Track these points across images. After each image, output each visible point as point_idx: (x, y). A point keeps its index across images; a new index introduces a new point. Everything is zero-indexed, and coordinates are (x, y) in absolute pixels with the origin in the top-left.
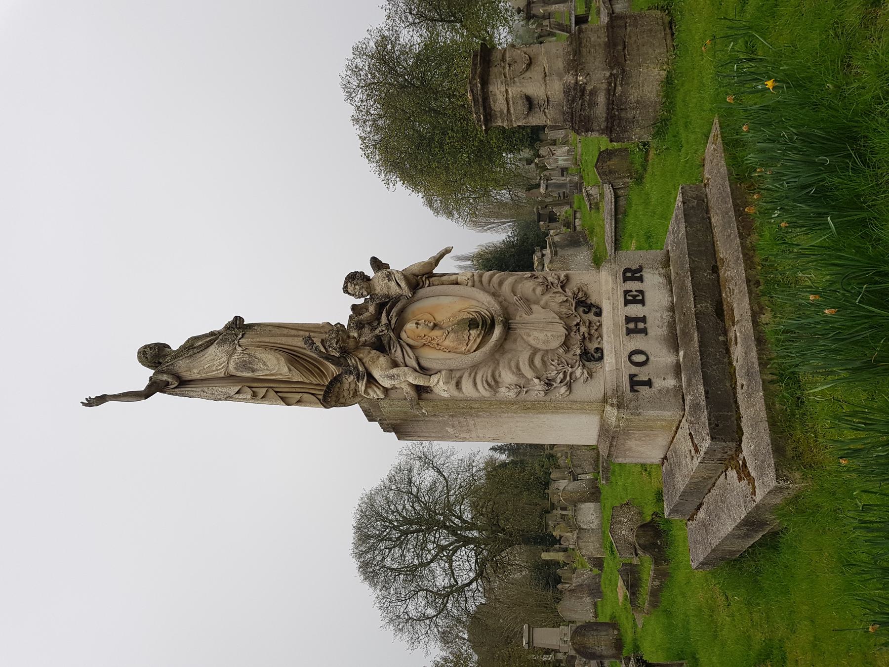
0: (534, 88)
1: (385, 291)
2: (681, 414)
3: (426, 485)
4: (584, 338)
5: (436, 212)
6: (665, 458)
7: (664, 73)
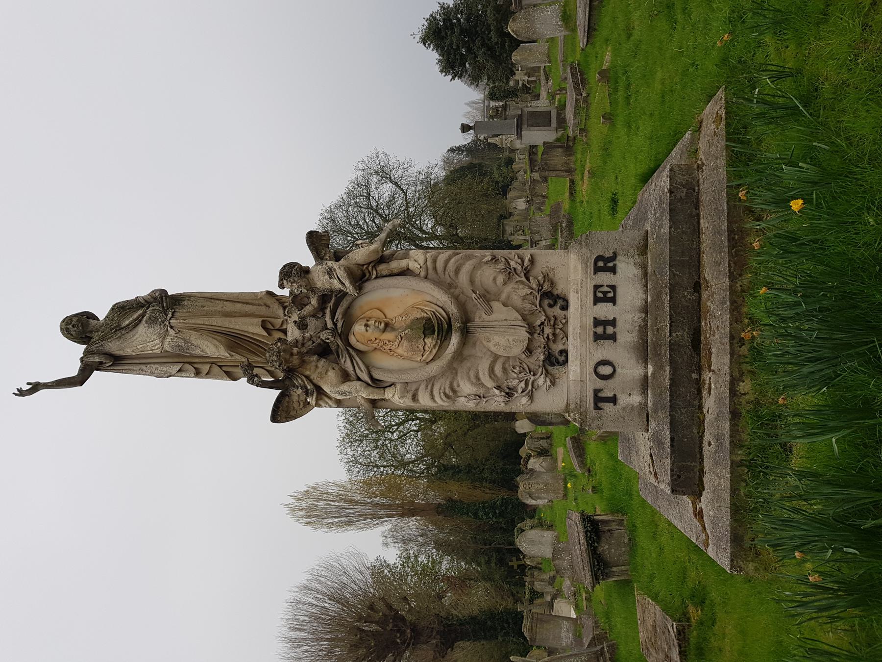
1: (327, 286)
3: (386, 197)
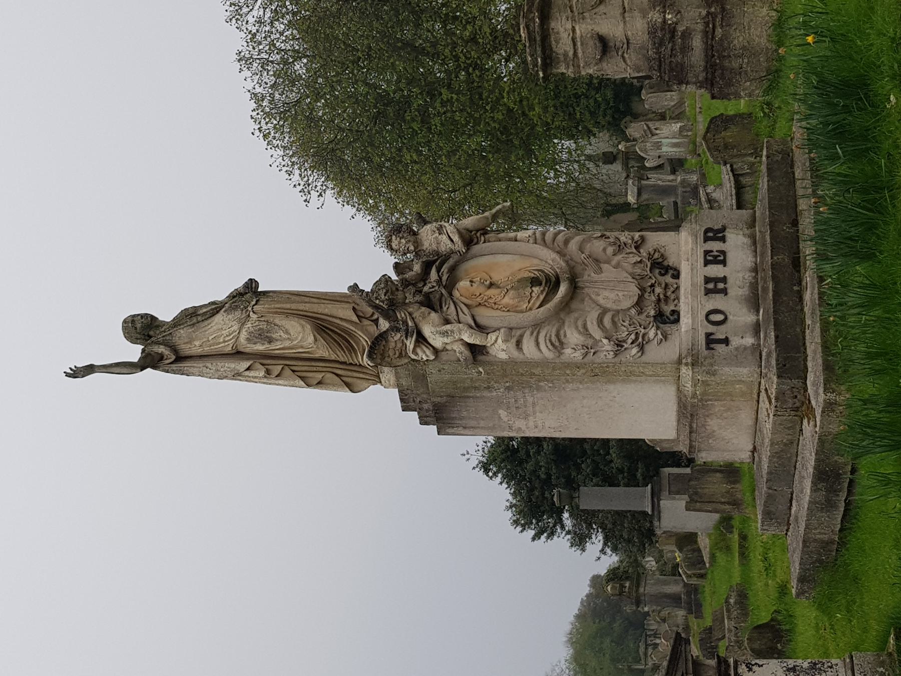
1: (434, 247)
2: (759, 371)
4: (659, 300)
6: (755, 448)
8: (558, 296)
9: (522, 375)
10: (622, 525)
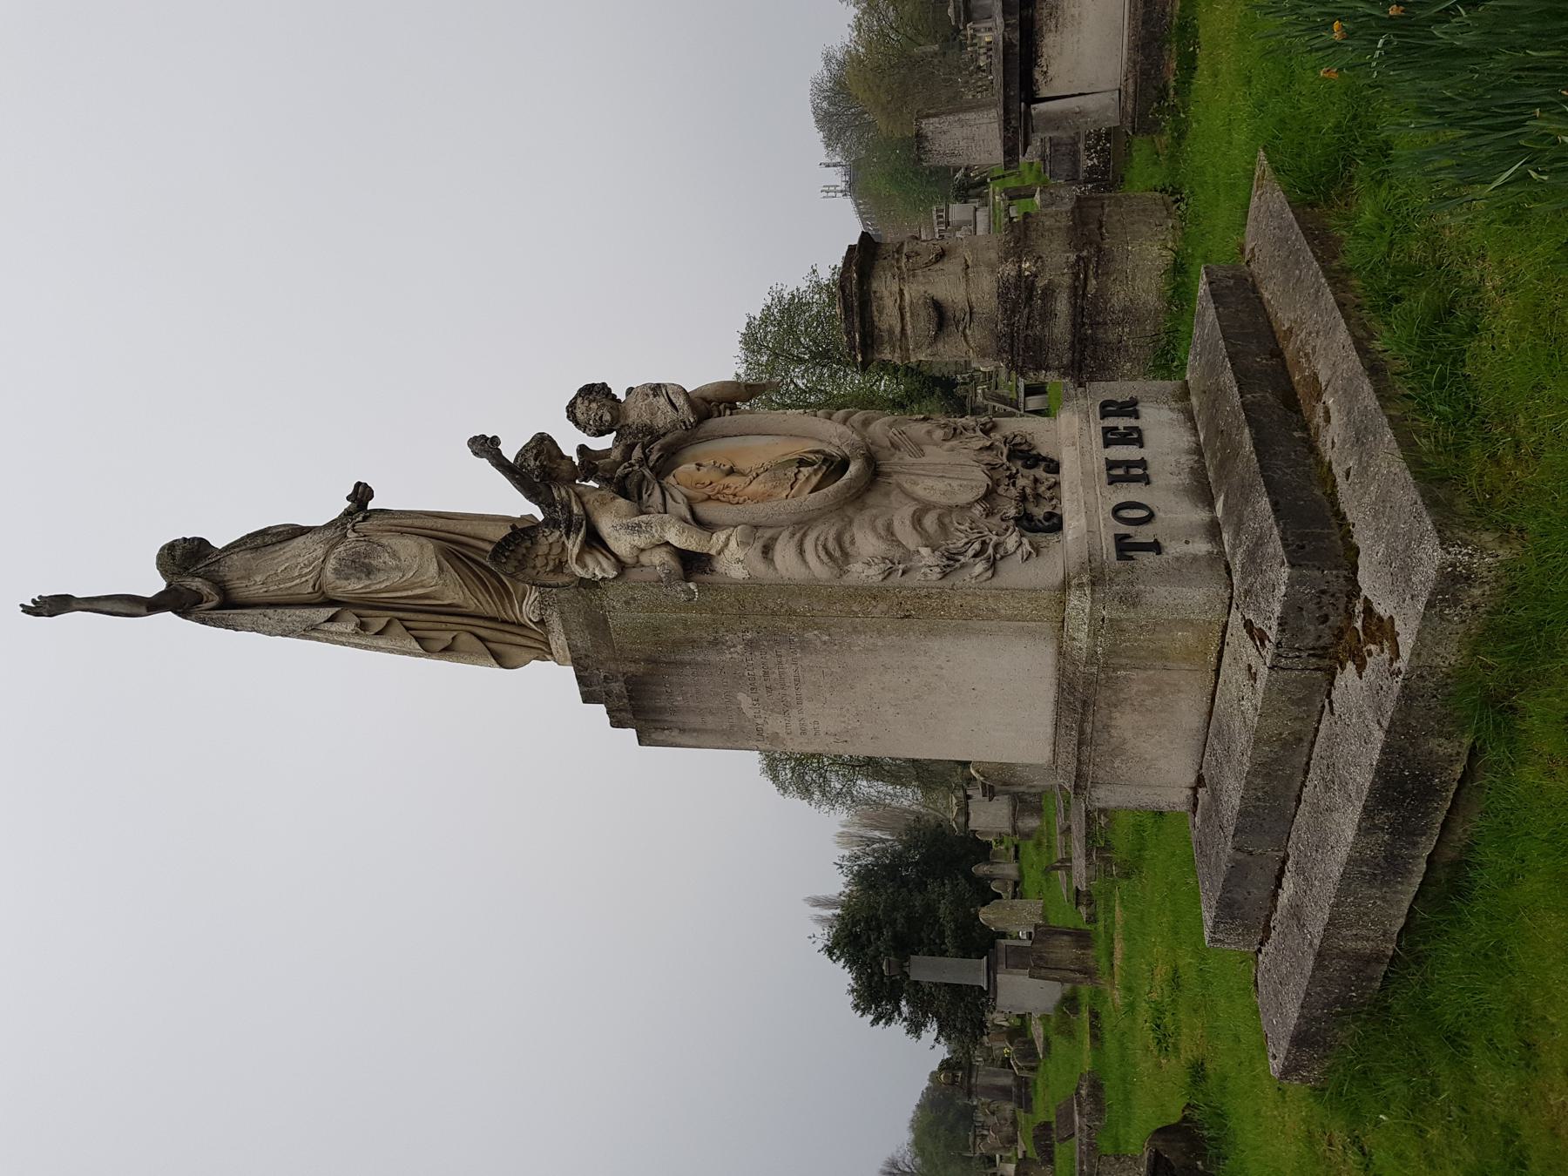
0: (947, 286)
1: (646, 419)
2: (1226, 595)
5: (783, 788)
6: (1200, 781)
7: (1169, 255)
8: (847, 475)
9: (774, 613)
10: (955, 1014)
